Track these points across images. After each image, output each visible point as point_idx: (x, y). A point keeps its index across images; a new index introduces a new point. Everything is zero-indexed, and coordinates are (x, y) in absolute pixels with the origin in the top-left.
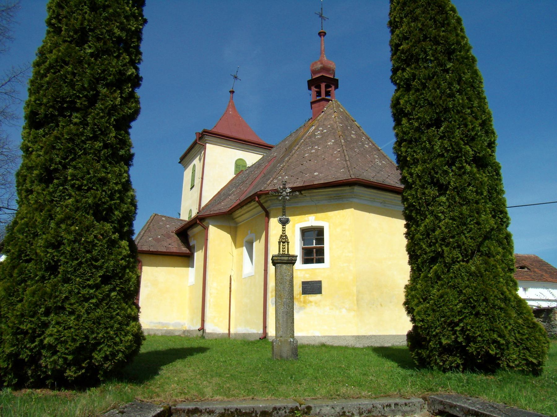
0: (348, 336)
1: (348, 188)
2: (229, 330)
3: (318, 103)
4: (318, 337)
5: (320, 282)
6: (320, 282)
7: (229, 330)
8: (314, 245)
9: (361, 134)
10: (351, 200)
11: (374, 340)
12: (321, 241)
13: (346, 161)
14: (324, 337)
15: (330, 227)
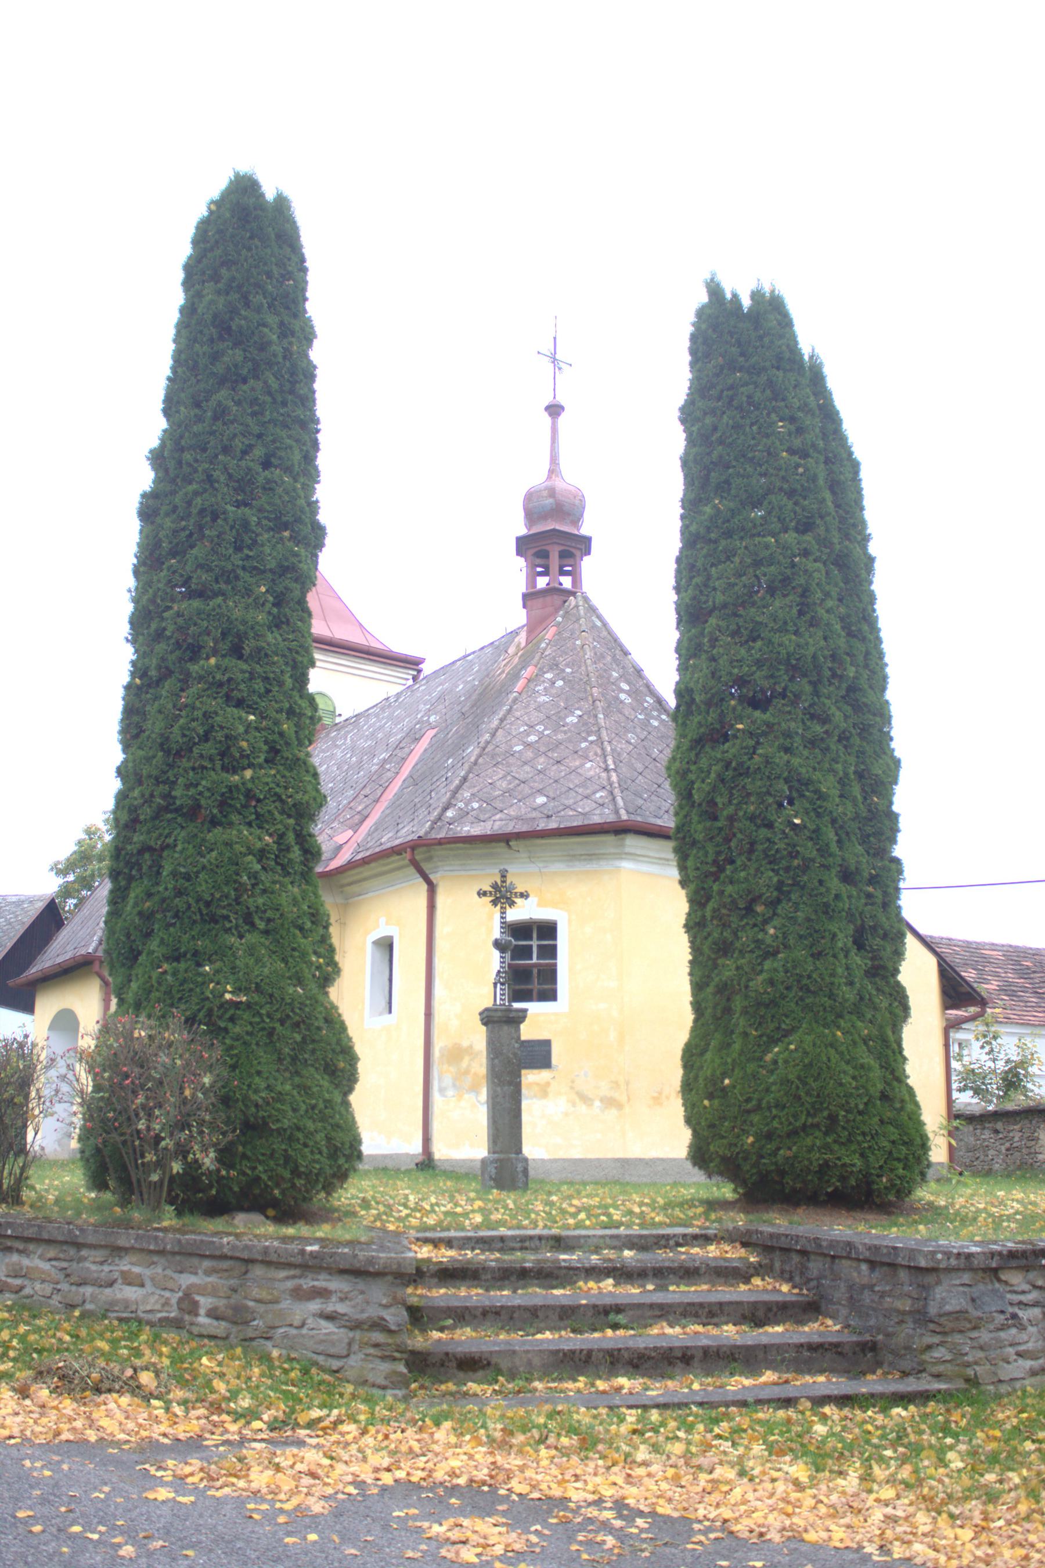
0: (607, 1160)
1: (610, 839)
2: (427, 1140)
3: (541, 600)
4: (543, 1160)
5: (547, 1043)
6: (547, 1043)
7: (427, 1140)
8: (535, 960)
9: (643, 689)
10: (617, 863)
11: (660, 1168)
12: (550, 952)
13: (606, 770)
14: (556, 1160)
15: (570, 921)
